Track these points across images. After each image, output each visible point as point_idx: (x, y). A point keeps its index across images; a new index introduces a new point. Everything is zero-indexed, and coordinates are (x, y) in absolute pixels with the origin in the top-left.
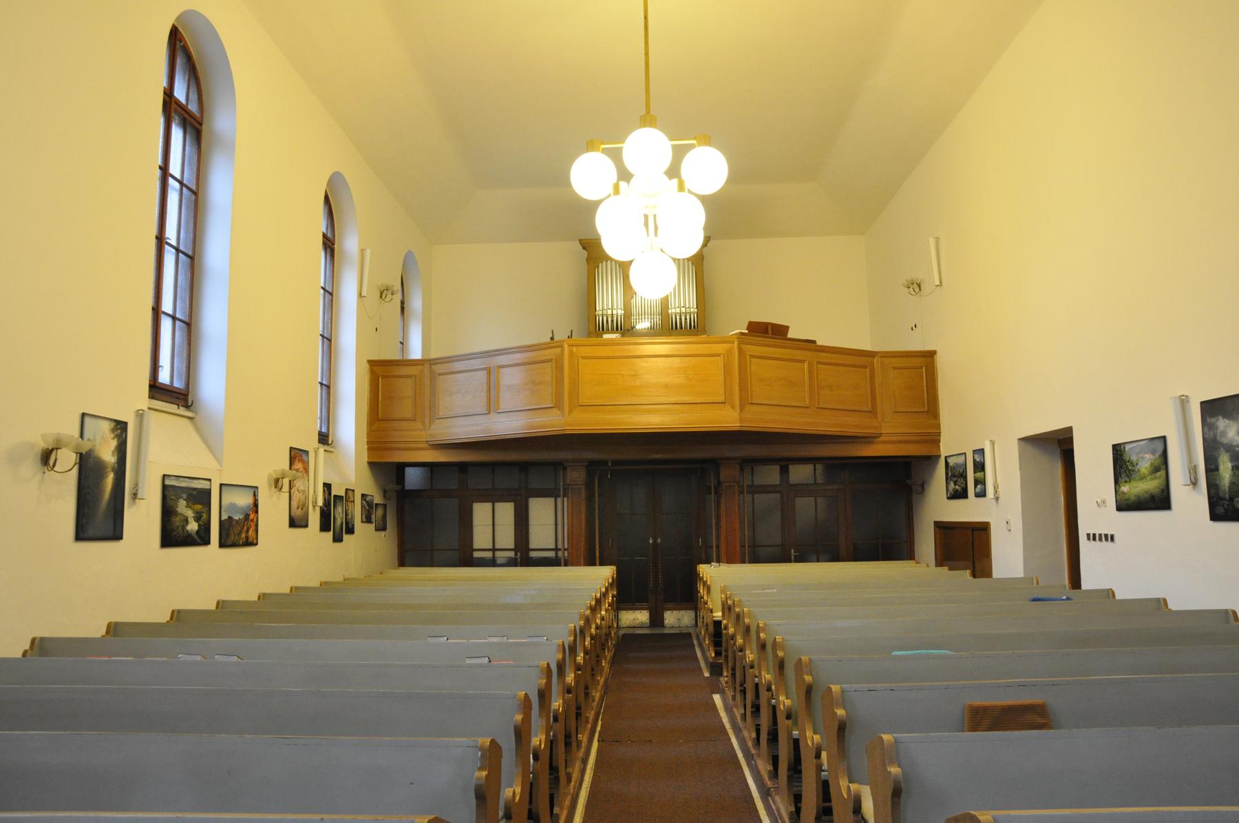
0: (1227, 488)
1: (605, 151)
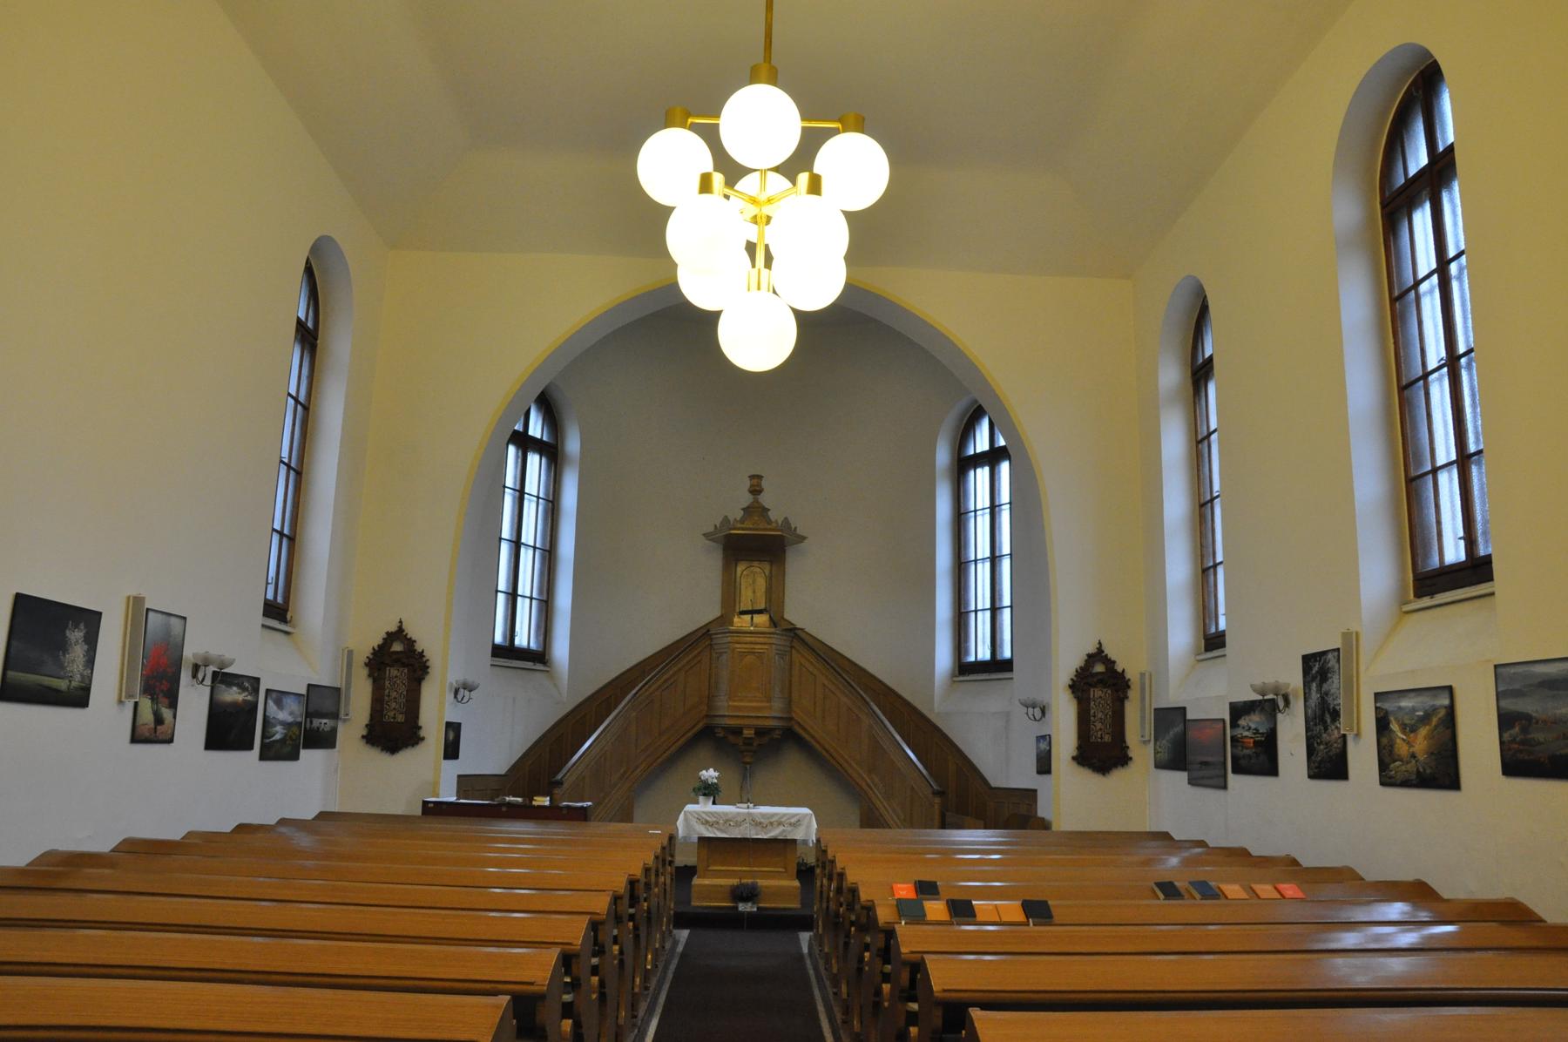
0: (1532, 736)
1: (695, 128)
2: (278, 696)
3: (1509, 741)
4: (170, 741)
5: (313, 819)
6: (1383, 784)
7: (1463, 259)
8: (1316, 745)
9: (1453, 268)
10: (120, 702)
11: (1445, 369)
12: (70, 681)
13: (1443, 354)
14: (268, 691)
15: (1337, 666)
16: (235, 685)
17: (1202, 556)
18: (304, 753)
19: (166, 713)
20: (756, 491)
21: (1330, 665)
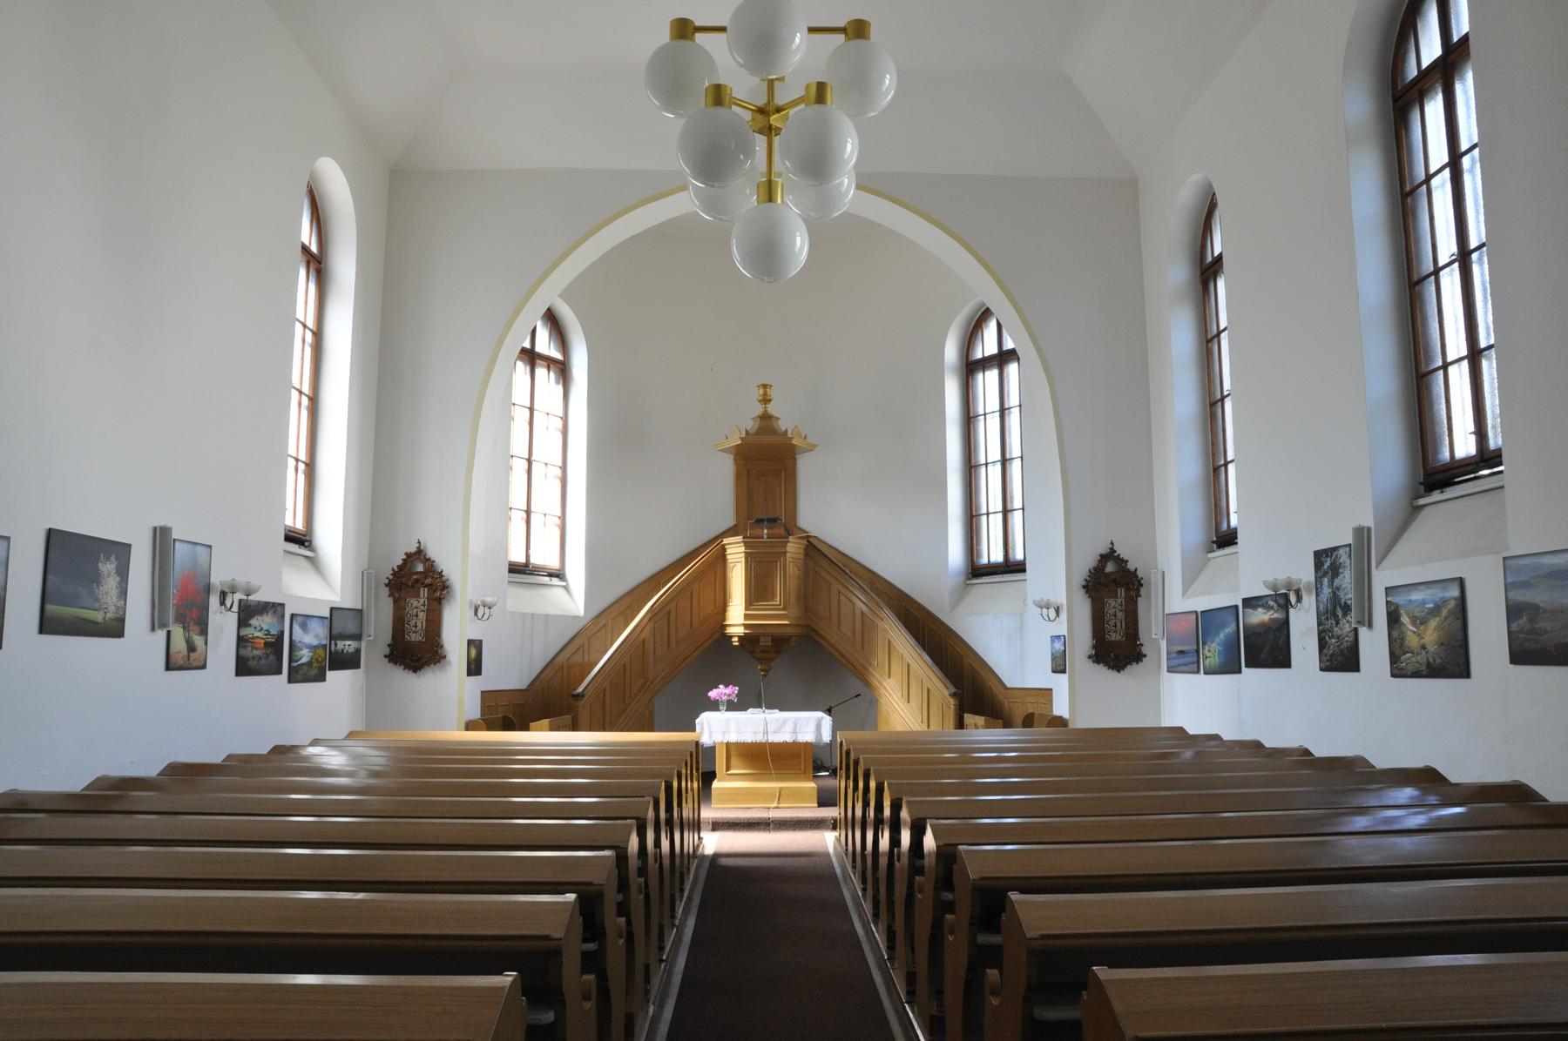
2: (304, 620)
3: (1516, 631)
4: (204, 667)
5: (269, 753)
6: (1393, 675)
7: (1476, 152)
8: (1327, 638)
9: (1466, 161)
10: (153, 629)
11: (1457, 264)
12: (105, 613)
13: (1454, 249)
14: (293, 616)
15: (1348, 561)
16: (1259, 606)
17: (1214, 455)
18: (330, 674)
19: (198, 640)
20: (766, 400)
21: (1341, 561)
